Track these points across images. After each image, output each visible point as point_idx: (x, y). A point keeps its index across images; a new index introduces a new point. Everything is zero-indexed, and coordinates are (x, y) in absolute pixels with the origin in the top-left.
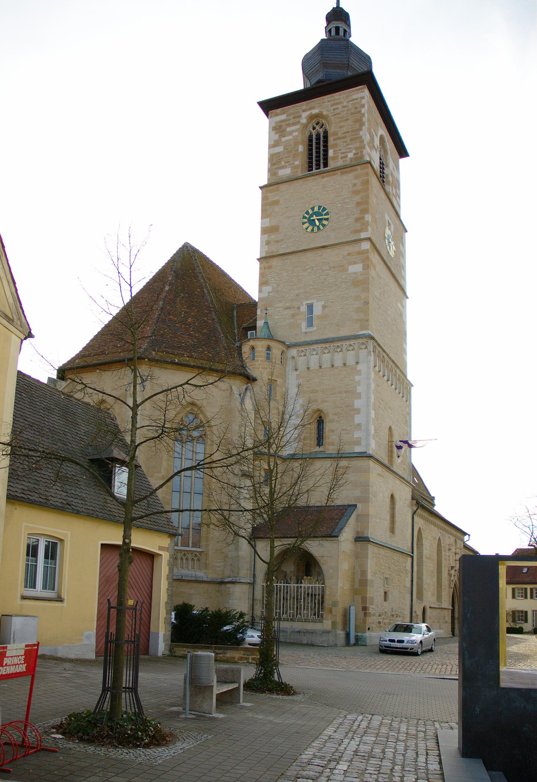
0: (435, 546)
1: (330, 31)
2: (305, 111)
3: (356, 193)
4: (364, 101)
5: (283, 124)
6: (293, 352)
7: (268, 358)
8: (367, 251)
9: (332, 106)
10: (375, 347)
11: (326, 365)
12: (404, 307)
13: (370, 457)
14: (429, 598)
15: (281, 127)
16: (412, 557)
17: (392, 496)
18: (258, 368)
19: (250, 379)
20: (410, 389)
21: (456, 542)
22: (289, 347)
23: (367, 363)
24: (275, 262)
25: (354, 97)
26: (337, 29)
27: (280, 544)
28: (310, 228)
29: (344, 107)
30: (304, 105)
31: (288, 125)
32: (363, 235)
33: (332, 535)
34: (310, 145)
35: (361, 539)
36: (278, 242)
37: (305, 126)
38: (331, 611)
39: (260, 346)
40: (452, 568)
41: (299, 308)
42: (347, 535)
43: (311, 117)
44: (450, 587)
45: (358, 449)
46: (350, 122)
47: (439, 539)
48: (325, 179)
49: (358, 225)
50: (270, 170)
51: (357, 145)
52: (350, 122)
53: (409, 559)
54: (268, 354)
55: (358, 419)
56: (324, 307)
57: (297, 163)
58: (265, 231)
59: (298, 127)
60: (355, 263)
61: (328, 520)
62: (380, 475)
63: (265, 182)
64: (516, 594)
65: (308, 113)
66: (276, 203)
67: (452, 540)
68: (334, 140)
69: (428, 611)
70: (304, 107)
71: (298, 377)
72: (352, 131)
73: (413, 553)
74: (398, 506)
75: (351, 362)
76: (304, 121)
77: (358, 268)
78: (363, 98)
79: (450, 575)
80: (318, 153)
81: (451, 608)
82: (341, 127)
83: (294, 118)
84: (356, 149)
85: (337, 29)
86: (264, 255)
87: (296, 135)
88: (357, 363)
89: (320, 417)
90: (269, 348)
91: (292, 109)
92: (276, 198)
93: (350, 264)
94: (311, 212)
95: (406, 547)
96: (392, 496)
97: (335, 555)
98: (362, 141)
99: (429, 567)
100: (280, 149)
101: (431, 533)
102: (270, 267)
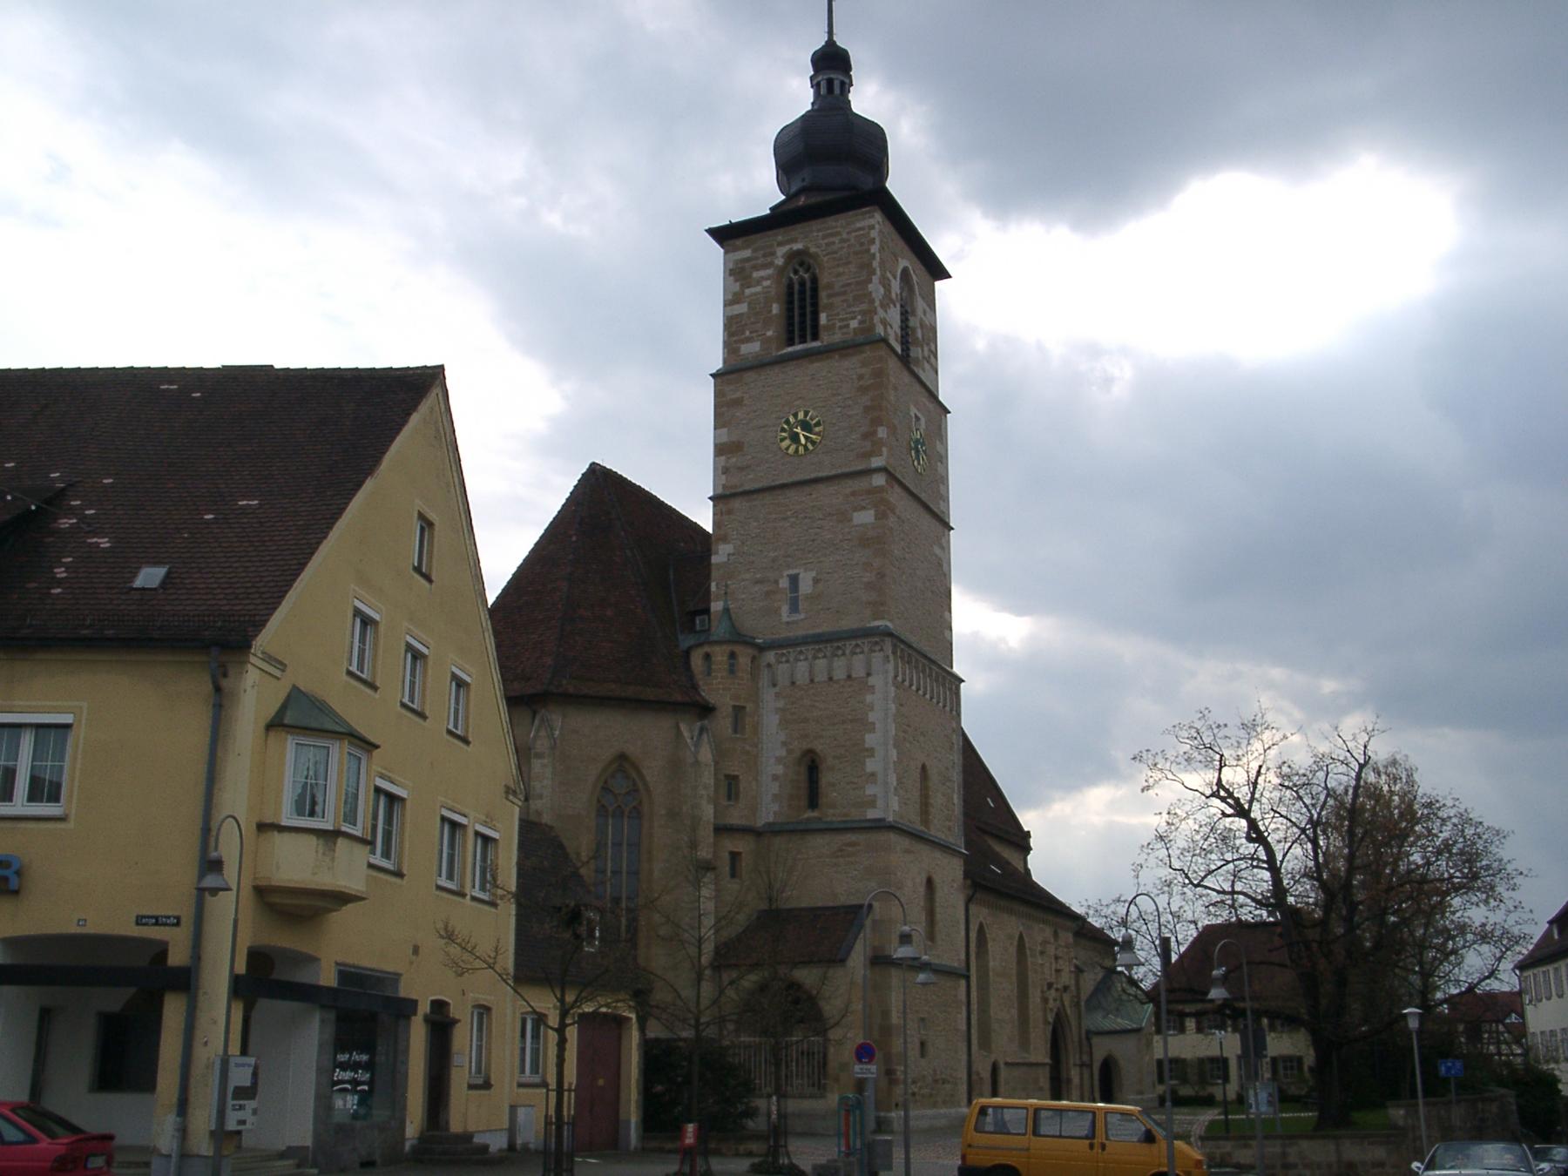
0: (1013, 950)
1: (818, 85)
2: (782, 248)
3: (863, 390)
4: (874, 234)
5: (747, 265)
6: (770, 656)
7: (732, 671)
8: (880, 489)
9: (824, 237)
10: (895, 646)
11: (821, 677)
12: (946, 548)
13: (892, 828)
14: (1004, 1045)
15: (743, 269)
16: (968, 978)
17: (930, 882)
18: (718, 690)
19: (705, 710)
20: (958, 688)
21: (1056, 934)
22: (762, 649)
23: (884, 680)
24: (737, 504)
25: (858, 225)
26: (830, 82)
27: (751, 980)
28: (793, 447)
29: (843, 241)
30: (780, 235)
31: (756, 268)
32: (876, 462)
33: (837, 959)
34: (790, 302)
35: (880, 961)
36: (741, 469)
37: (781, 271)
38: (837, 1080)
39: (720, 654)
40: (1050, 986)
41: (776, 582)
42: (858, 958)
43: (792, 256)
44: (1046, 1022)
45: (872, 814)
46: (852, 268)
47: (1021, 937)
48: (816, 365)
49: (868, 445)
50: (726, 344)
51: (864, 307)
52: (852, 268)
53: (963, 982)
54: (732, 665)
55: (871, 765)
56: (816, 581)
57: (769, 333)
58: (720, 450)
59: (769, 271)
60: (863, 508)
61: (832, 929)
62: (908, 851)
63: (719, 365)
64: (1164, 1023)
65: (787, 248)
66: (737, 403)
67: (1048, 932)
68: (829, 296)
69: (1003, 1073)
70: (780, 238)
71: (777, 695)
72: (858, 283)
73: (968, 969)
74: (940, 894)
75: (859, 672)
76: (780, 262)
77: (865, 517)
78: (872, 227)
79: (1045, 1000)
80: (803, 315)
81: (1048, 1060)
82: (839, 275)
83: (764, 256)
84: (863, 313)
85: (830, 82)
86: (720, 491)
87: (765, 282)
88: (869, 675)
89: (813, 761)
90: (733, 655)
91: (761, 240)
92: (738, 395)
93: (855, 509)
94: (792, 419)
95: (955, 959)
96: (930, 882)
97: (843, 989)
98: (872, 301)
99: (1003, 989)
100: (742, 308)
101: (1005, 929)
102: (730, 512)
